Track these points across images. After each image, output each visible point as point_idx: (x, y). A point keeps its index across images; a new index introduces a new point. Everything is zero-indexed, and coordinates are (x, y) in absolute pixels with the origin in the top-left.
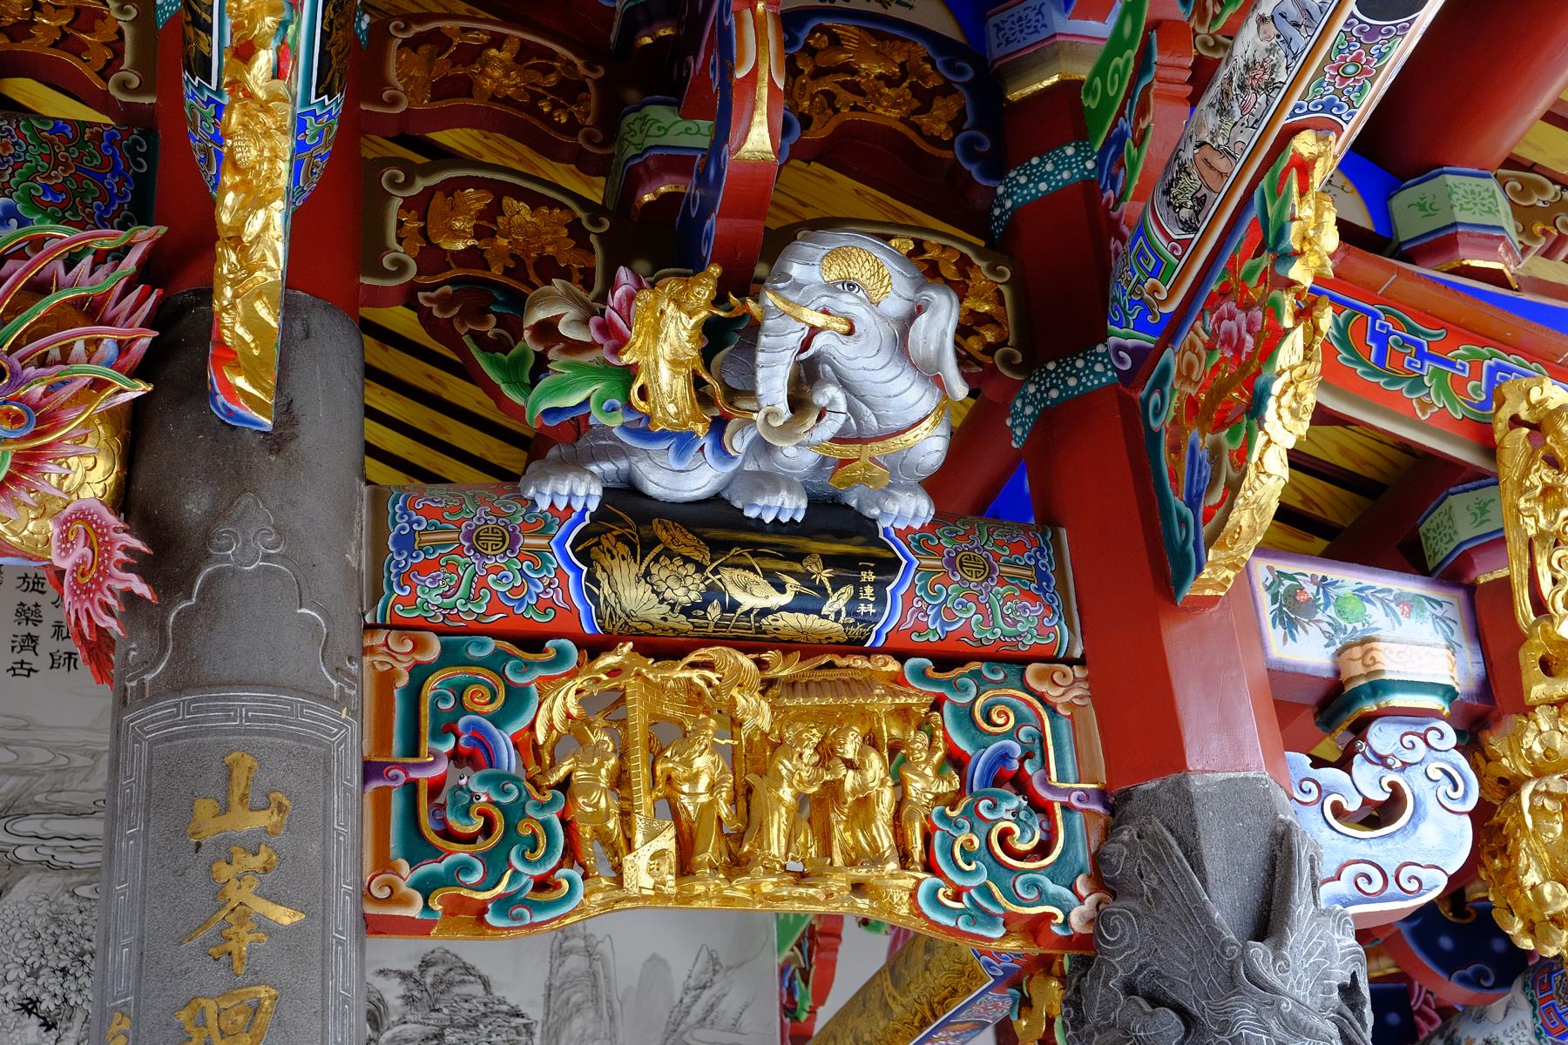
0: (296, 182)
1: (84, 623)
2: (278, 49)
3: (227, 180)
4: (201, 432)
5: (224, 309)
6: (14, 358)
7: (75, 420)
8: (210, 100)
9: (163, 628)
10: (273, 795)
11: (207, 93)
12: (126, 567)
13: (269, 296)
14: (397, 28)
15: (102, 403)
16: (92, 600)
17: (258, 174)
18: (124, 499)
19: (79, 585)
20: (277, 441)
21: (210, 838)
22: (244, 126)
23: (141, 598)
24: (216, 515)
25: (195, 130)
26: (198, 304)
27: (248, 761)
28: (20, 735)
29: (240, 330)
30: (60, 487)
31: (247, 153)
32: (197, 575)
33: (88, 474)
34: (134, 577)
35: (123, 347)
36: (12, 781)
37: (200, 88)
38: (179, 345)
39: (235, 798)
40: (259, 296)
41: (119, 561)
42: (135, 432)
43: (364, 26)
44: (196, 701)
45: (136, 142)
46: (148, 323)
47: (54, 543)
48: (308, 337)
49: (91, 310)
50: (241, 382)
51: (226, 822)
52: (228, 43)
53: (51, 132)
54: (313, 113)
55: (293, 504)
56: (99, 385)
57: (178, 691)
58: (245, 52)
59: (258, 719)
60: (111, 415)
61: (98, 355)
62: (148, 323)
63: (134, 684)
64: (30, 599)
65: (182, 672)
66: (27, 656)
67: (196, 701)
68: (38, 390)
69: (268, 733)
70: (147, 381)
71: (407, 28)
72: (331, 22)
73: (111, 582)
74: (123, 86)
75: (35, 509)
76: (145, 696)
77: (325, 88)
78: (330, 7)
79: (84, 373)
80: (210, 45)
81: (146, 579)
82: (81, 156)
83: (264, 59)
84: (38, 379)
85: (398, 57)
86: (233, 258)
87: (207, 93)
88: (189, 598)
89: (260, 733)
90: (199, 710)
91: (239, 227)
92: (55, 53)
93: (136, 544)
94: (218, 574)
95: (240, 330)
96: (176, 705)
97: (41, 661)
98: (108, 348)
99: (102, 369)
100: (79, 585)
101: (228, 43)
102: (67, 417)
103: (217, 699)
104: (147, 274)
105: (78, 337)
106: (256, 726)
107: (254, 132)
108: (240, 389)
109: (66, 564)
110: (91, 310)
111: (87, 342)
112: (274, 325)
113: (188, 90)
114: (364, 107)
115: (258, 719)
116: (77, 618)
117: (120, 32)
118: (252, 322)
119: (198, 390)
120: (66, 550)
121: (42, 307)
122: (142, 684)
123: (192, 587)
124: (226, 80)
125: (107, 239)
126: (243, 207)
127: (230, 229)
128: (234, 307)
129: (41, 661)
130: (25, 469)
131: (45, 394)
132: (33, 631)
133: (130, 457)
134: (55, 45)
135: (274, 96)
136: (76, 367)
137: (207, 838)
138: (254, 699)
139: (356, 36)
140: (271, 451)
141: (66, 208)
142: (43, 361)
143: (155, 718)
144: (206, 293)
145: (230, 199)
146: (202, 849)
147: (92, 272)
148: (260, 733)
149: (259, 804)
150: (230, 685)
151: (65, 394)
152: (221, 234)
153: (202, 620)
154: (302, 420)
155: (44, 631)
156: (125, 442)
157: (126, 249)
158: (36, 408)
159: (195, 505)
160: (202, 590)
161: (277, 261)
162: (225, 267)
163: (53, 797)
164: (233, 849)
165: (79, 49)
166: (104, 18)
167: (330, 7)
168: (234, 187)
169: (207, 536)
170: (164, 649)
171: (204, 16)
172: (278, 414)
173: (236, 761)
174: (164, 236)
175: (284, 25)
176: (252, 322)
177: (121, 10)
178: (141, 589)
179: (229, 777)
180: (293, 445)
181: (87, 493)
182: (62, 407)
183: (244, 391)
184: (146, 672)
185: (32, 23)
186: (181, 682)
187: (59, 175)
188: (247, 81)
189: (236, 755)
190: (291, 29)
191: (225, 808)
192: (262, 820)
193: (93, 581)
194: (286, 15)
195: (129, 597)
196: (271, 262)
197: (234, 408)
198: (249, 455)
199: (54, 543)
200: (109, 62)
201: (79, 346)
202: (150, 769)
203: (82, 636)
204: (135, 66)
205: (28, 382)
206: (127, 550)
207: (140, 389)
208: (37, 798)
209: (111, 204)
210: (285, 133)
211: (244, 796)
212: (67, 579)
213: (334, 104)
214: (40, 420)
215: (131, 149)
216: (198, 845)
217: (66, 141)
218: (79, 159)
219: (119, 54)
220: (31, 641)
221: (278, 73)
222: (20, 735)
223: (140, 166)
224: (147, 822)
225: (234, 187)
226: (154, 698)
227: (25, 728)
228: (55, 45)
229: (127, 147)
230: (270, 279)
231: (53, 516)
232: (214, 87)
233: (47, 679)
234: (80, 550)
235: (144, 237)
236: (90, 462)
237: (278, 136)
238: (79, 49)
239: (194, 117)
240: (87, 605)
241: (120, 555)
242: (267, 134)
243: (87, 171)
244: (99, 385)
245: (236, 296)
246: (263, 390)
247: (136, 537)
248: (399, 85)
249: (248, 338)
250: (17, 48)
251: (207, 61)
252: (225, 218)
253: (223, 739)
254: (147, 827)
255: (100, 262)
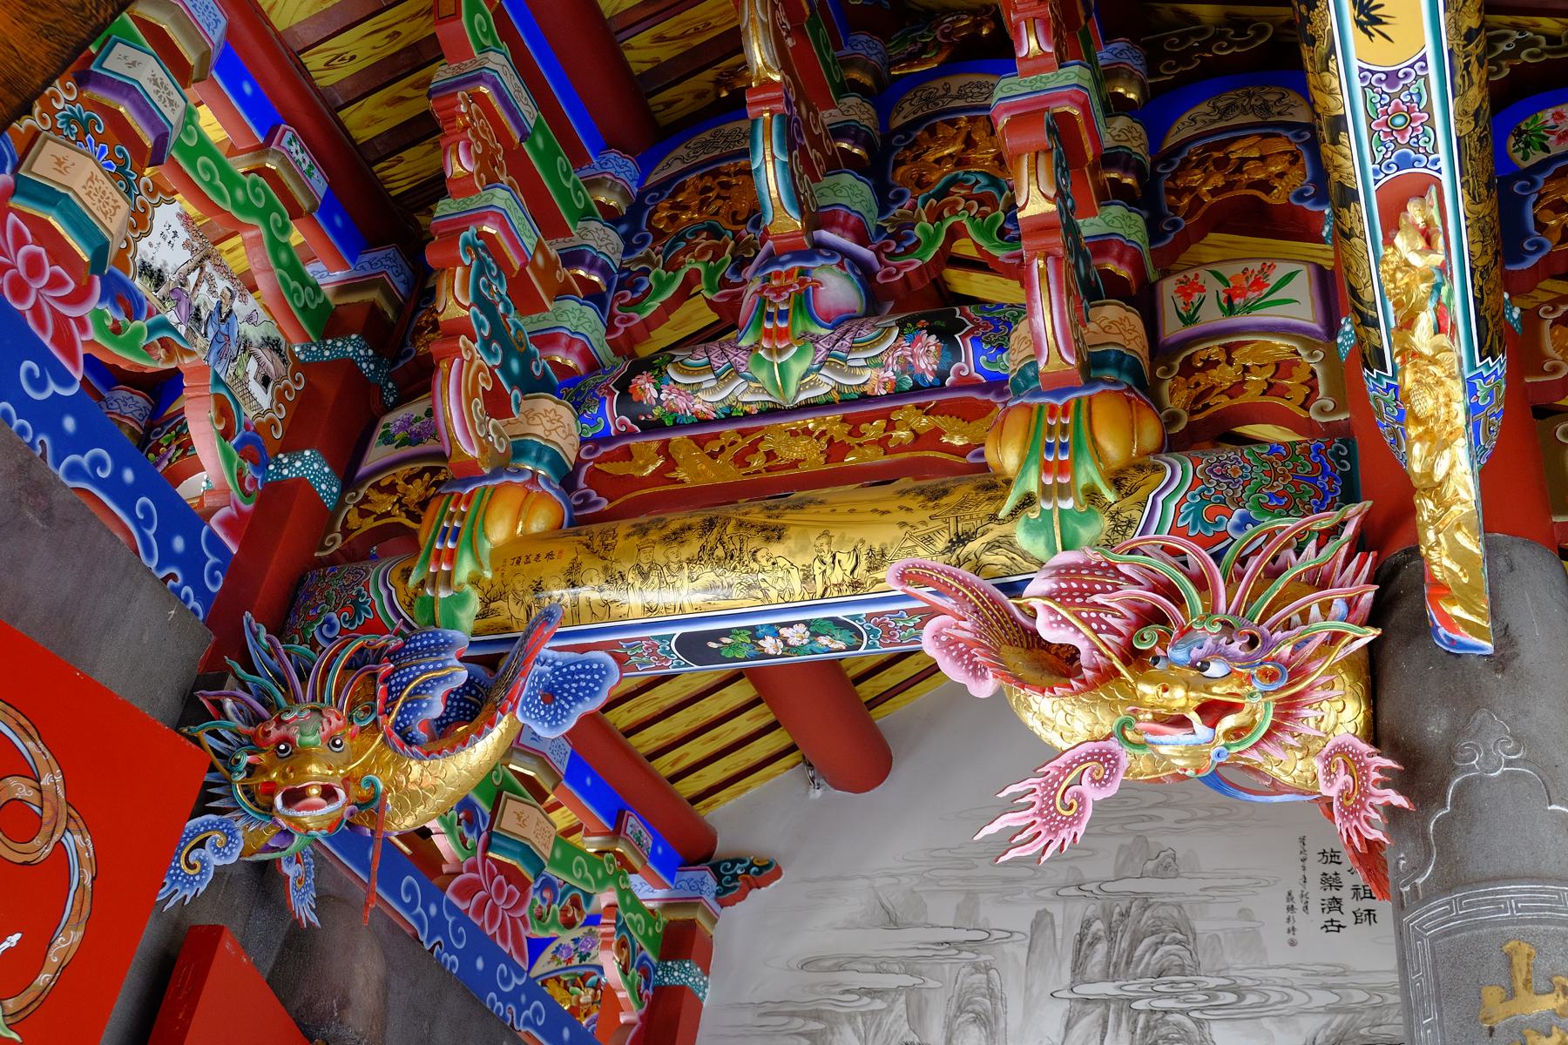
0: (1477, 442)
1: (1355, 839)
2: (1435, 309)
3: (1413, 431)
4: (1430, 664)
5: (1430, 548)
6: (1264, 627)
7: (1318, 671)
8: (1389, 386)
9: (1425, 836)
10: (1555, 979)
11: (1385, 381)
12: (1385, 785)
13: (1468, 525)
14: (1546, 312)
15: (1339, 653)
16: (1358, 818)
17: (1437, 420)
18: (1374, 733)
19: (1346, 808)
20: (1500, 661)
21: (1501, 1024)
22: (1418, 381)
23: (1400, 809)
24: (1456, 732)
25: (1382, 418)
26: (1410, 560)
27: (1526, 948)
28: (1339, 980)
29: (1446, 562)
30: (1318, 728)
31: (1424, 404)
32: (1448, 785)
33: (1339, 714)
34: (1390, 792)
35: (1351, 604)
36: (1339, 1018)
37: (1378, 379)
38: (1398, 593)
39: (1520, 984)
40: (1458, 527)
41: (1376, 781)
42: (1373, 672)
43: (1515, 316)
44: (1466, 897)
45: (1338, 449)
46: (1371, 580)
47: (1321, 777)
48: (1512, 569)
49: (1319, 580)
50: (1457, 611)
51: (1513, 1006)
52: (1393, 324)
53: (1270, 453)
54: (1480, 375)
55: (1526, 713)
56: (1336, 637)
57: (1449, 890)
58: (1408, 324)
59: (1528, 909)
60: (1349, 663)
61: (1332, 614)
62: (1371, 580)
63: (1407, 889)
64: (1330, 869)
65: (1450, 873)
66: (1335, 915)
67: (1466, 897)
68: (1286, 650)
69: (1540, 921)
70: (1375, 626)
71: (1555, 310)
72: (1481, 289)
73: (1372, 800)
74: (1322, 411)
75: (1300, 749)
76: (1420, 898)
77: (1488, 352)
78: (1477, 275)
79: (1321, 628)
80: (1380, 337)
81: (1401, 791)
82: (1295, 466)
83: (1426, 320)
84: (1286, 641)
85: (1552, 334)
86: (1430, 505)
87: (1385, 381)
88: (1445, 807)
89: (1532, 922)
90: (1470, 905)
91: (1429, 474)
92: (1266, 399)
93: (1388, 763)
94: (1467, 783)
95: (1446, 562)
96: (1449, 903)
97: (1347, 919)
98: (1339, 607)
99: (1337, 622)
100: (1346, 808)
101: (1393, 324)
102: (1313, 669)
103: (1485, 894)
104: (1360, 544)
105: (1313, 601)
106: (1528, 915)
107: (1427, 385)
108: (1460, 619)
109: (1333, 792)
110: (1319, 580)
111: (1320, 604)
112: (1477, 551)
113: (1370, 384)
114: (1528, 380)
115: (1528, 909)
116: (1349, 836)
117: (1313, 372)
118: (1457, 553)
119: (1421, 628)
120: (1331, 781)
121: (1280, 583)
122: (1414, 887)
123: (1445, 797)
124: (1396, 350)
125: (1324, 521)
126: (1429, 454)
127: (1422, 476)
128: (1438, 543)
129: (1347, 919)
130: (1286, 717)
131: (1292, 653)
132: (1337, 894)
133: (1373, 695)
134: (1264, 393)
135: (1440, 349)
136: (1315, 626)
137: (1499, 1024)
138: (1521, 891)
139: (1509, 325)
140: (1496, 671)
141: (1289, 505)
142: (1288, 626)
143: (1432, 916)
144: (1414, 551)
145: (1417, 450)
146: (1496, 1033)
147: (1317, 553)
148: (1532, 922)
149: (1544, 988)
150: (1496, 880)
151: (1309, 649)
152: (1416, 483)
153: (1459, 825)
154: (1521, 640)
155: (1345, 894)
156: (1367, 686)
157: (1344, 523)
158: (1287, 665)
159: (1435, 727)
160: (1454, 799)
161: (1469, 491)
162: (1425, 514)
163: (1375, 1030)
164: (1526, 1031)
165: (1282, 392)
166: (1298, 365)
167: (1477, 275)
168: (1419, 438)
169: (1451, 752)
170: (1430, 854)
171: (1371, 313)
172: (1497, 639)
173: (1514, 949)
174: (1371, 509)
175: (1437, 287)
176: (1457, 553)
177: (1311, 355)
178: (1399, 800)
179: (1510, 964)
180: (1516, 663)
181: (1340, 731)
182: (1309, 660)
183: (1461, 621)
184: (1417, 876)
185: (1244, 382)
186: (1447, 883)
187: (1280, 485)
188: (1412, 343)
189: (1512, 944)
190: (1444, 290)
191: (1511, 994)
192: (1549, 1003)
193: (1357, 801)
194: (1437, 278)
195: (1391, 811)
196: (1463, 495)
197: (1455, 637)
198: (1477, 677)
199: (1321, 777)
200: (1307, 396)
201: (1315, 611)
202: (1435, 962)
203: (1354, 848)
204: (1329, 394)
205: (1277, 644)
206: (1381, 770)
207: (1371, 634)
208: (1362, 1032)
209: (1325, 499)
210: (1454, 378)
211: (1527, 981)
212: (1336, 804)
213: (1499, 365)
214: (1292, 675)
215: (1336, 455)
216: (1492, 1030)
217: (1282, 458)
218: (1294, 469)
219: (1314, 389)
220: (1336, 903)
221: (1439, 329)
222: (1339, 980)
223: (1344, 466)
224: (1440, 1011)
225: (1419, 438)
226: (1427, 899)
227: (1343, 974)
228: (1264, 393)
229: (1332, 454)
230: (1466, 510)
231: (1316, 754)
232: (1390, 374)
233: (1353, 931)
234: (1343, 778)
235: (1354, 513)
236: (1339, 705)
237: (1449, 382)
238: (1282, 392)
239: (1379, 407)
240: (1355, 823)
241: (1376, 775)
242: (1439, 383)
243: (1302, 478)
244: (1336, 637)
245: (1437, 533)
246: (1479, 615)
247: (1389, 757)
248: (1558, 356)
249: (1456, 568)
250: (1236, 402)
251: (1380, 352)
252: (1417, 468)
253: (1498, 930)
254: (1440, 1015)
255: (1321, 542)
